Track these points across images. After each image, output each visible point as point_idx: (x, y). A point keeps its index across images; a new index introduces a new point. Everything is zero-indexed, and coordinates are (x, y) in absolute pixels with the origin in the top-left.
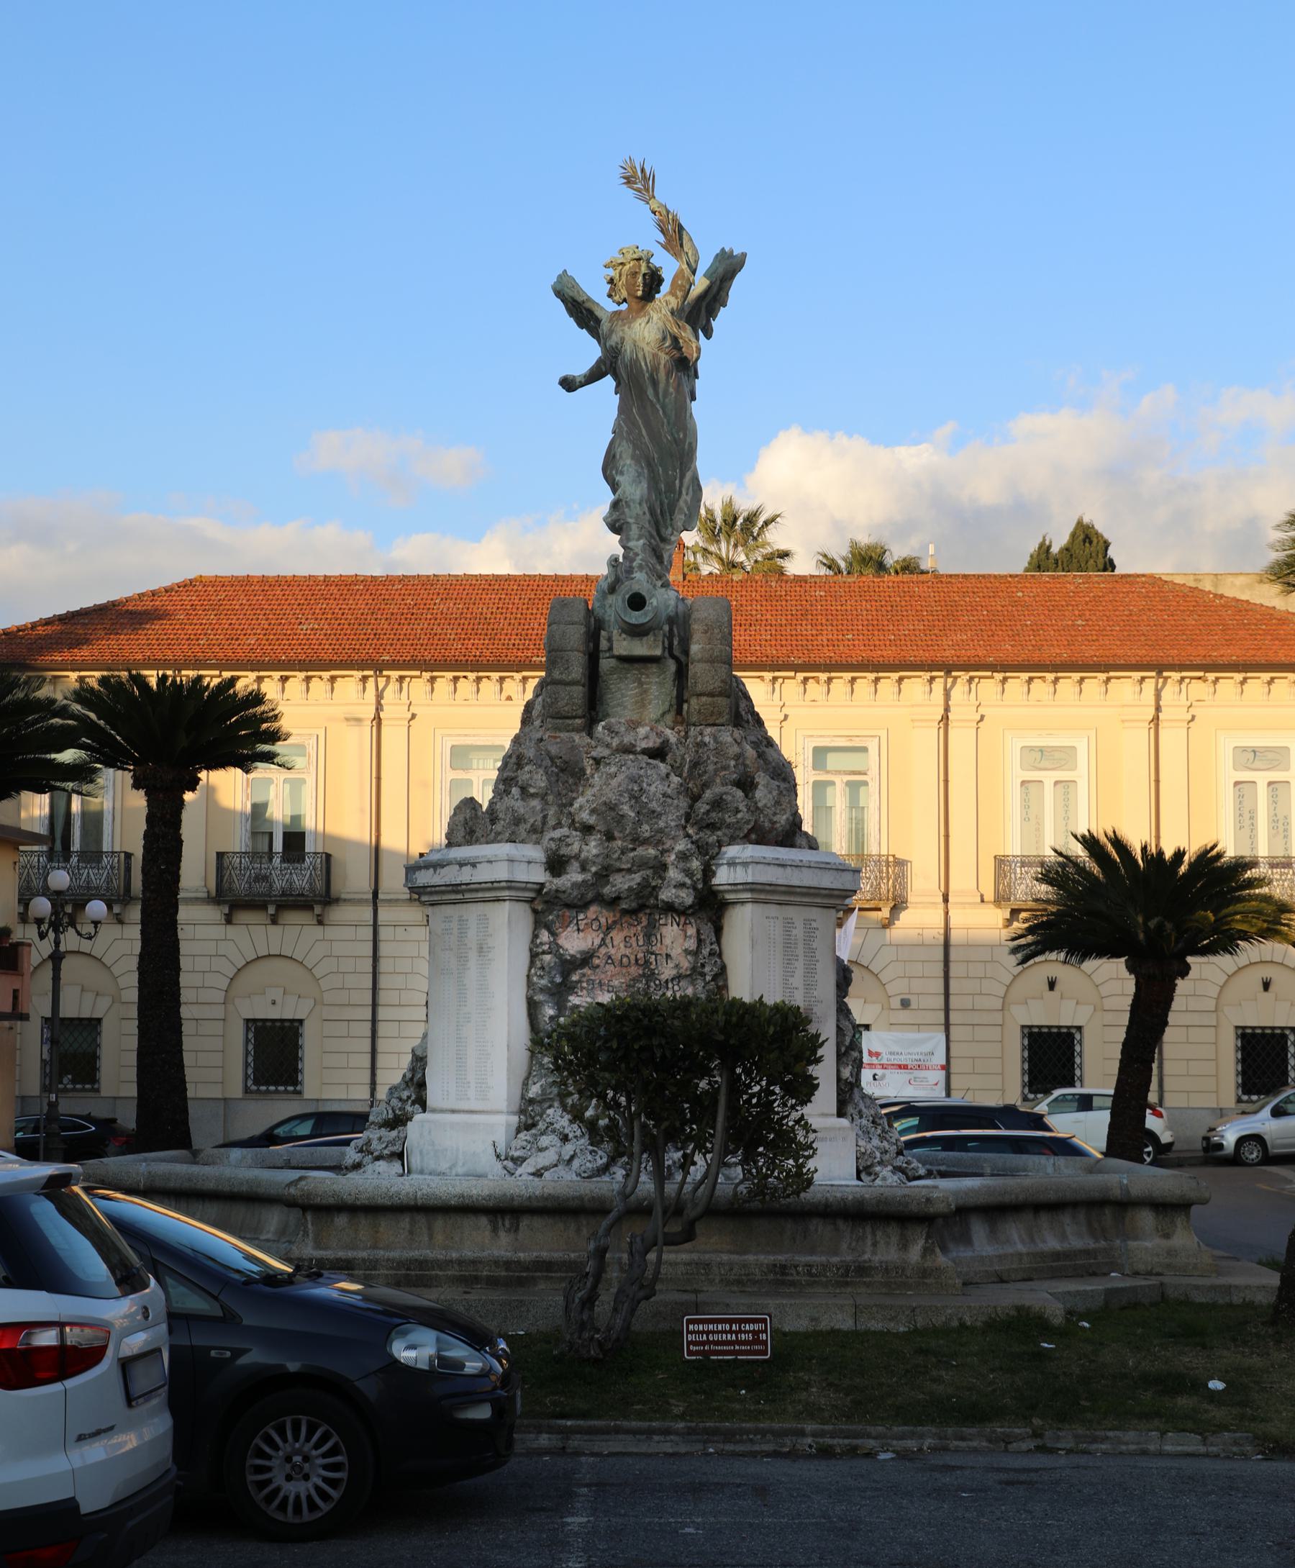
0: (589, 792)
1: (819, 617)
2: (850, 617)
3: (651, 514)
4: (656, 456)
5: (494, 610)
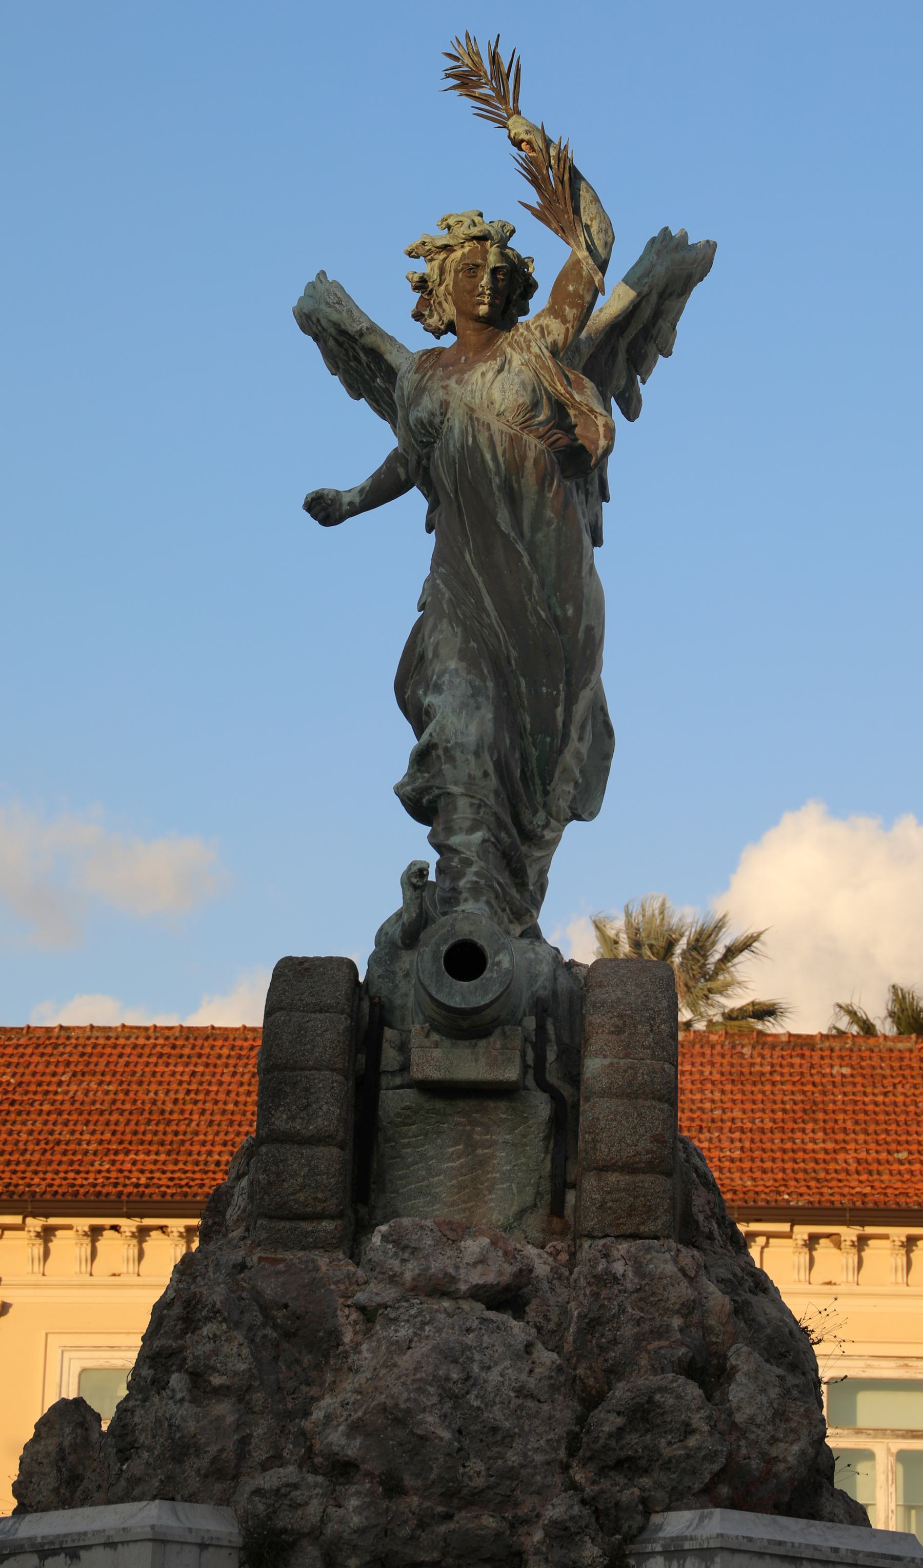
0: (349, 1384)
1: (841, 1117)
2: (902, 1118)
3: (501, 778)
4: (514, 653)
5: (181, 1096)
